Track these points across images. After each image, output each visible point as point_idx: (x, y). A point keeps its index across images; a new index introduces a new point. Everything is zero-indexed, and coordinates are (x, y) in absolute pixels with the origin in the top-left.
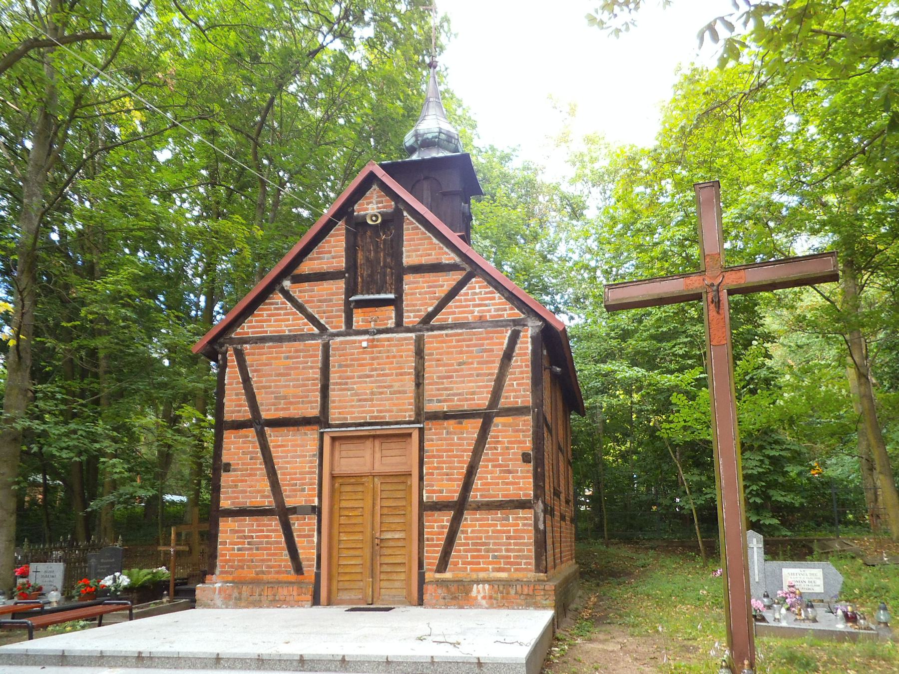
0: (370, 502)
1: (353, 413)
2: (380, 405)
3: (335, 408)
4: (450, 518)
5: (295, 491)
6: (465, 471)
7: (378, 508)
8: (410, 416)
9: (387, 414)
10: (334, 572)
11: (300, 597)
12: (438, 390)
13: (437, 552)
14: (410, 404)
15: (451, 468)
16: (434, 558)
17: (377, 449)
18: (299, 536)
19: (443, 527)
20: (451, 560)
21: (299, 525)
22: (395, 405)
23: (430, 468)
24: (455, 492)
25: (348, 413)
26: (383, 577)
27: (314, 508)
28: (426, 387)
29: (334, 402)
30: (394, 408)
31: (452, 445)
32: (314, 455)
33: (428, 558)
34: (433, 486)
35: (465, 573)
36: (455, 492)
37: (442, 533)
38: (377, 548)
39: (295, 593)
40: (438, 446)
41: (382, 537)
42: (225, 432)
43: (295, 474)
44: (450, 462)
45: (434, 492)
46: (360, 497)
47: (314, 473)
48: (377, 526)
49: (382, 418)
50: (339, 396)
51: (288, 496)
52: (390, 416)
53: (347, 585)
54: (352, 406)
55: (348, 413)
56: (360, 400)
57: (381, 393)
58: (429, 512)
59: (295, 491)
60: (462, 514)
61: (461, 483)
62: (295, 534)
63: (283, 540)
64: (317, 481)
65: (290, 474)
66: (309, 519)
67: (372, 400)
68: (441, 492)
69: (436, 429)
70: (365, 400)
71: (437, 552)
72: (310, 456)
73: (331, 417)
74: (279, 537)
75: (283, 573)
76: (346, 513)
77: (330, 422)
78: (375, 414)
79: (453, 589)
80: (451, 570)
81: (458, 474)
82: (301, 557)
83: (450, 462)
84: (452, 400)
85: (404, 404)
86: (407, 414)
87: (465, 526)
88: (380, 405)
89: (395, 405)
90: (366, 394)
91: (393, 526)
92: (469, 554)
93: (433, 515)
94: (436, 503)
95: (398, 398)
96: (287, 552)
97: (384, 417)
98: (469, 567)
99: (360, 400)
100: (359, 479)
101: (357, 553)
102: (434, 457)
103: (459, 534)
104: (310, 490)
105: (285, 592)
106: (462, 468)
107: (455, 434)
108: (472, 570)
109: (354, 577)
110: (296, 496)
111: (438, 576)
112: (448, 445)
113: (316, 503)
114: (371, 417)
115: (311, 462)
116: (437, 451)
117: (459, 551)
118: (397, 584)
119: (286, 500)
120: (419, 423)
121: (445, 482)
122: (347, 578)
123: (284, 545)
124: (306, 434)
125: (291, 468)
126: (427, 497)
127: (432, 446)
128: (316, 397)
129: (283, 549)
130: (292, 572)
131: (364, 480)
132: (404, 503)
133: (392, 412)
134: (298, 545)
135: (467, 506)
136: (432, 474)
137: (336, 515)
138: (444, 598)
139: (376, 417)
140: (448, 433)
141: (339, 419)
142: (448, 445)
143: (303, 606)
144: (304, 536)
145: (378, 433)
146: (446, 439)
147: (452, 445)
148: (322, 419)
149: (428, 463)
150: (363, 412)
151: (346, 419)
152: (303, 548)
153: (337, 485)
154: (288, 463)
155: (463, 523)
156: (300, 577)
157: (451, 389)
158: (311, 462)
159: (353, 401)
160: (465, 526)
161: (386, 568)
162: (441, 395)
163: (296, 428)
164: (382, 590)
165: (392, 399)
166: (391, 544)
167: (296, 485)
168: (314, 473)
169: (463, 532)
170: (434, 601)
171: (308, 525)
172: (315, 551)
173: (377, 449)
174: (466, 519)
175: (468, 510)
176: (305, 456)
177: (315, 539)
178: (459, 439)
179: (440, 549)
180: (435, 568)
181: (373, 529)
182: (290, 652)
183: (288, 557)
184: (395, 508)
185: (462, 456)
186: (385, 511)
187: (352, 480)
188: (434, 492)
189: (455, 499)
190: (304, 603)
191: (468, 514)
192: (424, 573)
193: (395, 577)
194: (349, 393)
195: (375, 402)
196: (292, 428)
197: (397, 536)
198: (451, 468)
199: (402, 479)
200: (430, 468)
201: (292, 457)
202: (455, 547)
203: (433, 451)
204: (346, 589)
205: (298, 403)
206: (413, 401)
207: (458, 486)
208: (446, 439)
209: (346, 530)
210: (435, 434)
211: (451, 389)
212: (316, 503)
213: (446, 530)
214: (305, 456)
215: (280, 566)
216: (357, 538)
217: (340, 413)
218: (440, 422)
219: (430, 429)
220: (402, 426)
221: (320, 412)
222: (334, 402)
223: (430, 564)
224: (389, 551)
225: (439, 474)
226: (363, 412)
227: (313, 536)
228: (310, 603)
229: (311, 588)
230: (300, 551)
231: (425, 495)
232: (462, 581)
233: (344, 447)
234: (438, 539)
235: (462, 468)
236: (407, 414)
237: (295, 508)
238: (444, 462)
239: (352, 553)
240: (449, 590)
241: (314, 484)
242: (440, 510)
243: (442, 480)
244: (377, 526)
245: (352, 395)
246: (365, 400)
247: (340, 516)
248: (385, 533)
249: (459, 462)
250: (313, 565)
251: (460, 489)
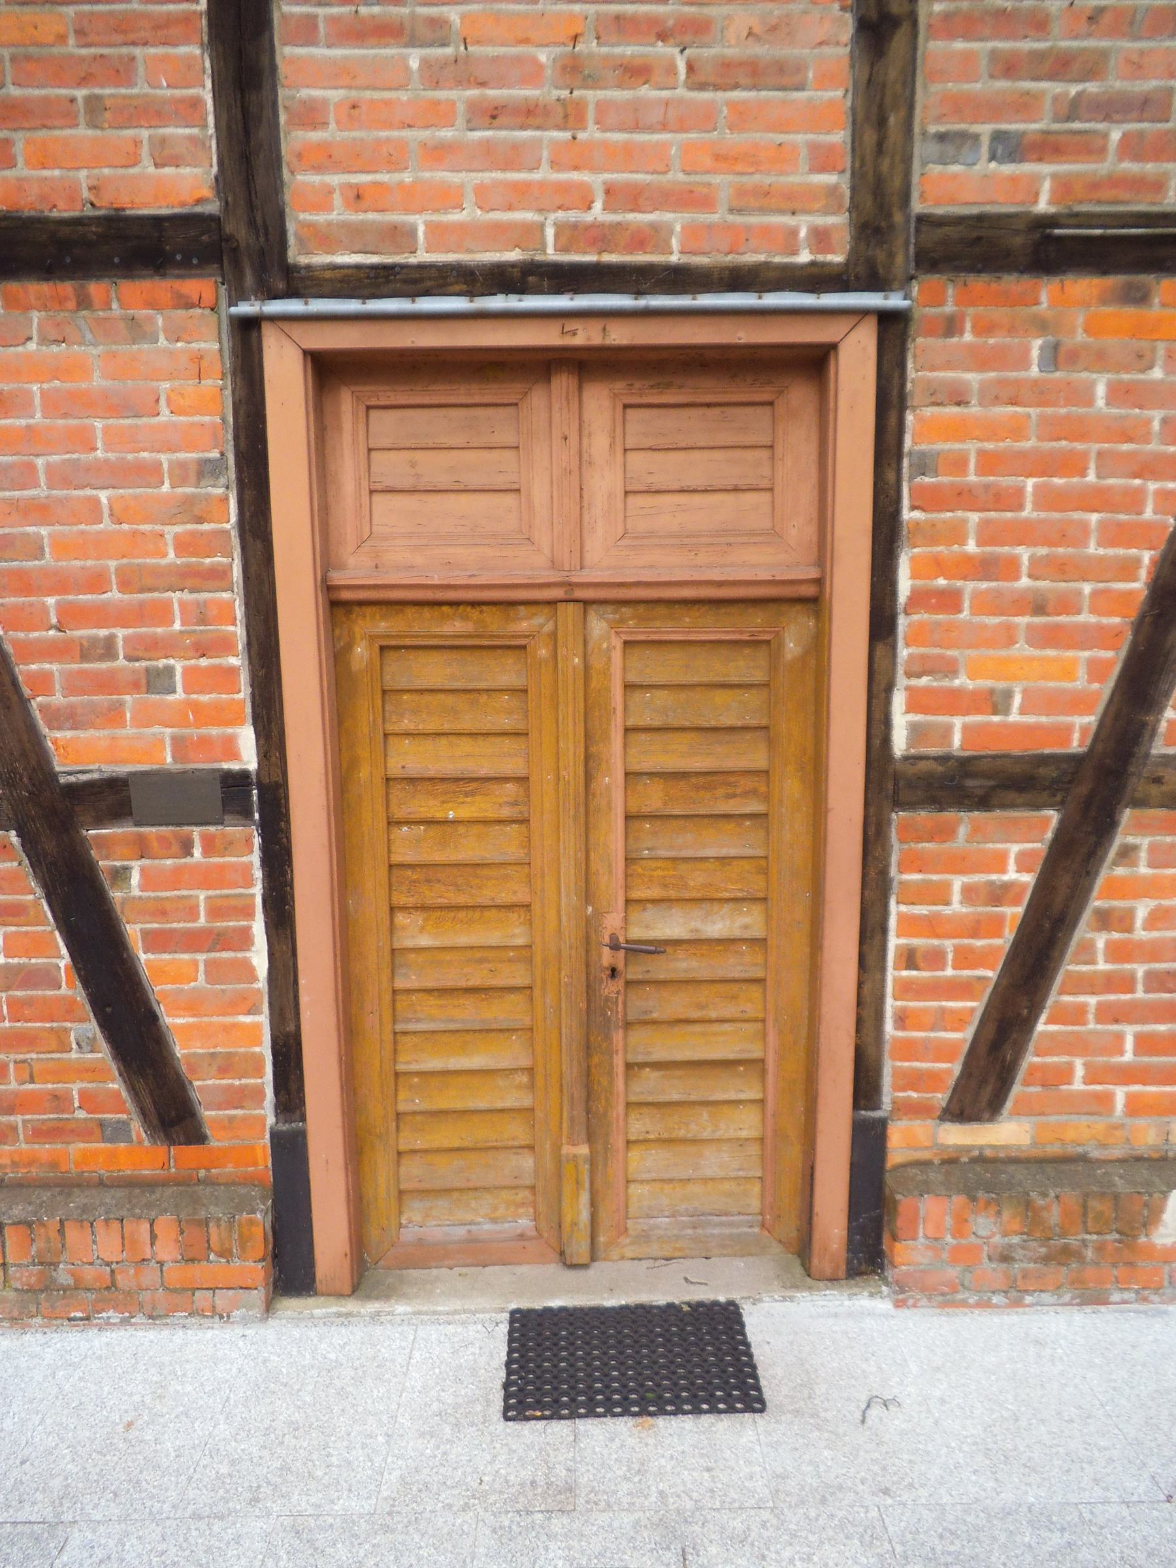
0: (572, 750)
1: (450, 198)
2: (627, 156)
3: (325, 158)
4: (1040, 847)
5: (106, 683)
6: (1139, 585)
7: (612, 780)
8: (820, 238)
9: (676, 221)
10: (376, 1112)
11: (197, 1272)
12: (1009, 67)
13: (958, 1021)
14: (822, 160)
15: (1061, 569)
16: (942, 1051)
17: (599, 443)
18: (156, 941)
19: (999, 894)
20: (1031, 1059)
21: (148, 881)
22: (724, 159)
23: (939, 566)
24: (1077, 703)
25: (413, 198)
26: (638, 1126)
27: (235, 783)
28: (933, 48)
29: (312, 116)
30: (722, 182)
31: (1079, 430)
32: (207, 470)
33: (908, 1050)
34: (951, 669)
35: (1099, 1124)
36: (1077, 703)
37: (994, 926)
38: (611, 988)
39: (167, 1250)
40: (991, 431)
41: (636, 933)
42: (1127, 815)
43: (97, 582)
44: (1062, 536)
45: (954, 702)
46: (506, 723)
47: (218, 576)
48: (611, 884)
49: (640, 239)
50: (341, 74)
51: (58, 718)
52: (692, 231)
53: (447, 1171)
54: (438, 153)
55: (413, 198)
56: (493, 114)
57: (637, 72)
58: (923, 816)
59: (106, 683)
60: (1105, 826)
61: (1114, 657)
62: (133, 931)
63: (64, 960)
64: (239, 631)
65: (60, 584)
66: (209, 847)
67: (571, 116)
68: (997, 702)
69: (984, 329)
70: (530, 114)
71: (958, 1021)
72: (180, 474)
73: (297, 220)
74: (39, 945)
75: (82, 1132)
76: (426, 806)
77: (296, 256)
78: (597, 212)
79: (1054, 1216)
80: (1025, 1109)
81: (1100, 603)
82: (179, 1051)
83: (1062, 536)
84: (1092, 147)
85: (782, 157)
86: (803, 225)
87: (1116, 889)
88: (627, 156)
89: (724, 159)
90: (532, 73)
91: (697, 879)
92: (1129, 1032)
93: (947, 833)
94: (965, 766)
95: (741, 117)
96: (92, 1027)
97: (652, 237)
98: (1120, 1094)
99: (493, 114)
100: (493, 621)
101: (498, 1012)
102: (964, 498)
103: (1083, 931)
104: (194, 680)
105: (107, 1244)
106: (1127, 569)
107: (1100, 361)
108: (1135, 1107)
109: (481, 1133)
110: (114, 716)
111: (956, 1136)
112: (1056, 429)
113: (248, 758)
114: (570, 234)
115: (191, 510)
116: (988, 463)
117: (1077, 1015)
118: (714, 1162)
119: (55, 738)
120: (875, 282)
121: (1022, 649)
122: (446, 1136)
123: (71, 990)
124: (137, 330)
125: (62, 547)
126: (916, 731)
127: (960, 430)
128: (183, 74)
129: (69, 1011)
130: (137, 1127)
131: (525, 624)
132: (757, 758)
133: (705, 202)
134: (160, 990)
135: (1137, 785)
136: (949, 601)
137: (371, 817)
138: (1005, 1258)
139: (600, 236)
140: (1054, 356)
141: (355, 235)
142: (1056, 429)
143: (222, 1316)
144: (194, 941)
145: (620, 335)
146: (1041, 394)
147: (1079, 430)
148: (237, 229)
149: (931, 535)
150: (520, 195)
151: (401, 236)
152: (193, 1005)
153: (361, 652)
154: (41, 511)
155: (1110, 871)
156: (182, 1157)
157: (1093, 67)
158: (191, 510)
159: (439, 114)
160: (1116, 889)
161: (649, 1085)
162: (1025, 105)
163: (67, 288)
164: (635, 1190)
165: (705, 119)
166: (683, 965)
167: (108, 649)
168: (218, 576)
169: (1105, 920)
170: (953, 1272)
171: (207, 878)
172: (263, 1019)
173: (599, 443)
174: (1127, 853)
175: (1139, 803)
176: (149, 473)
177: (259, 958)
178: (1119, 394)
179: (975, 1006)
180: (941, 1098)
181: (588, 896)
182: (297, 917)
183: (103, 1054)
184: (712, 778)
185: (1134, 501)
186: (653, 798)
187: (456, 626)
188: (954, 702)
189: (1076, 745)
190: (222, 1299)
191: (1141, 828)
192: (882, 1124)
193: (702, 1124)
194: (414, 59)
195: (591, 133)
196: (35, 289)
197: (718, 925)
198: (1061, 569)
199: (755, 622)
200: (939, 566)
201: (59, 477)
202: (1057, 997)
203: (959, 464)
204: (447, 1191)
205: (65, 113)
206: (840, 137)
207: (1096, 670)
208: (1041, 394)
209: (431, 895)
210: (981, 360)
211: (1093, 67)
212: (248, 758)
213: (1014, 912)
214: (149, 473)
215: (59, 1101)
216: (494, 938)
217: (357, 197)
218: (1012, 283)
219: (951, 327)
220: (772, 300)
221: (221, 182)
222: (312, 116)
223: (914, 1080)
224: (677, 1004)
225: (984, 605)
226: (520, 195)
227: (244, 939)
228: (258, 1296)
229: (261, 1218)
230: (171, 1020)
231: (901, 722)
232: (1083, 1159)
233: (386, 425)
234: (965, 958)
235: (1127, 569)
236: (803, 225)
237: (115, 785)
238: (1025, 534)
239: (468, 1012)
240: (1031, 1217)
241: (225, 646)
242: (984, 803)
243: (1008, 636)
244: (611, 884)
245: (434, 75)
246: (530, 114)
247: (392, 823)
248: (651, 913)
249: (1114, 535)
250: (258, 1060)
251: (1105, 689)
